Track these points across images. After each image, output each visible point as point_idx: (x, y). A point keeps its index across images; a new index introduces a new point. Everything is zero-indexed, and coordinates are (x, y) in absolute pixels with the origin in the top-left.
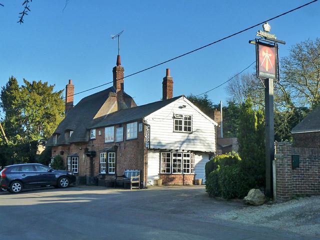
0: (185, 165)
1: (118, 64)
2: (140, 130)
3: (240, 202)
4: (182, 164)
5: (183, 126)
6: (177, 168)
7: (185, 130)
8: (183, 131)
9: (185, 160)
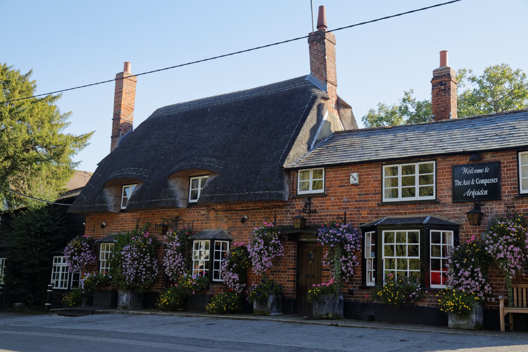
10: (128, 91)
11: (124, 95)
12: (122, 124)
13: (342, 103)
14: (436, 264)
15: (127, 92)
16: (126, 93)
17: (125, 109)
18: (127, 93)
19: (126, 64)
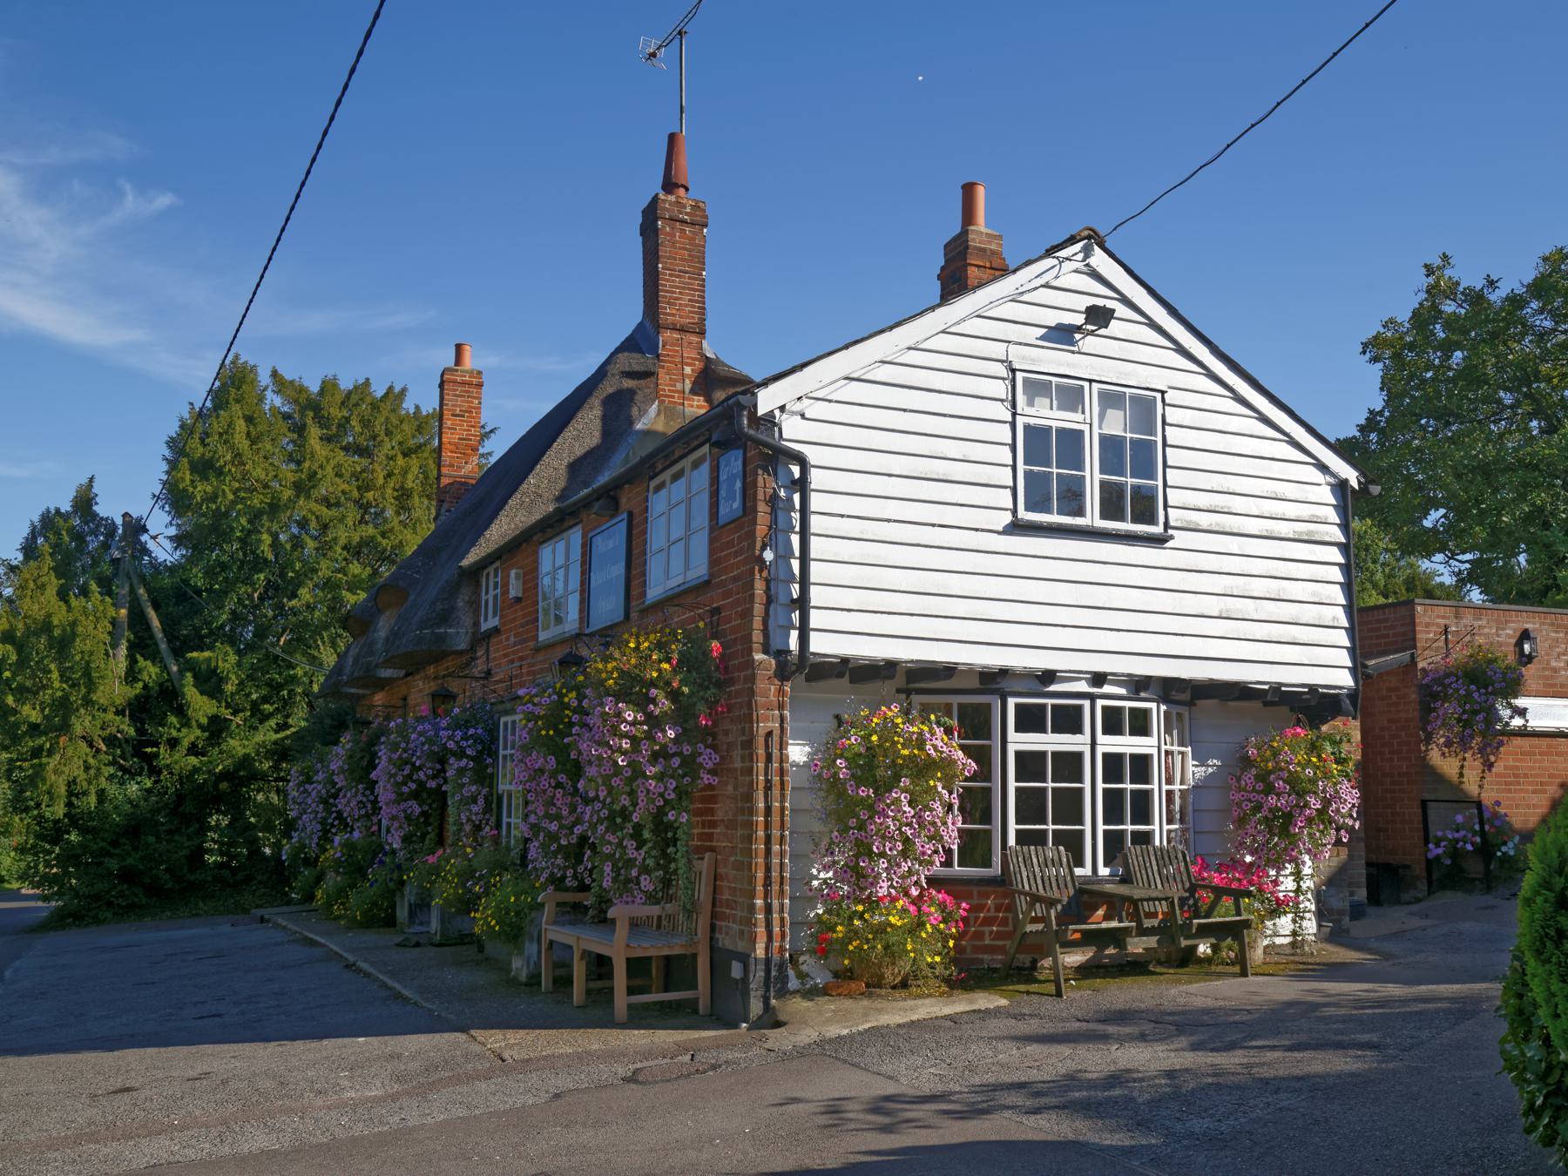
0: (1114, 800)
1: (669, 185)
2: (724, 510)
3: (1224, 999)
4: (1093, 787)
5: (1093, 477)
6: (1050, 785)
7: (1111, 507)
8: (1092, 517)
9: (1113, 764)
10: (458, 409)
11: (448, 419)
12: (445, 487)
13: (566, 524)
14: (729, 904)
15: (458, 412)
16: (453, 415)
17: (452, 452)
18: (456, 416)
19: (459, 348)
